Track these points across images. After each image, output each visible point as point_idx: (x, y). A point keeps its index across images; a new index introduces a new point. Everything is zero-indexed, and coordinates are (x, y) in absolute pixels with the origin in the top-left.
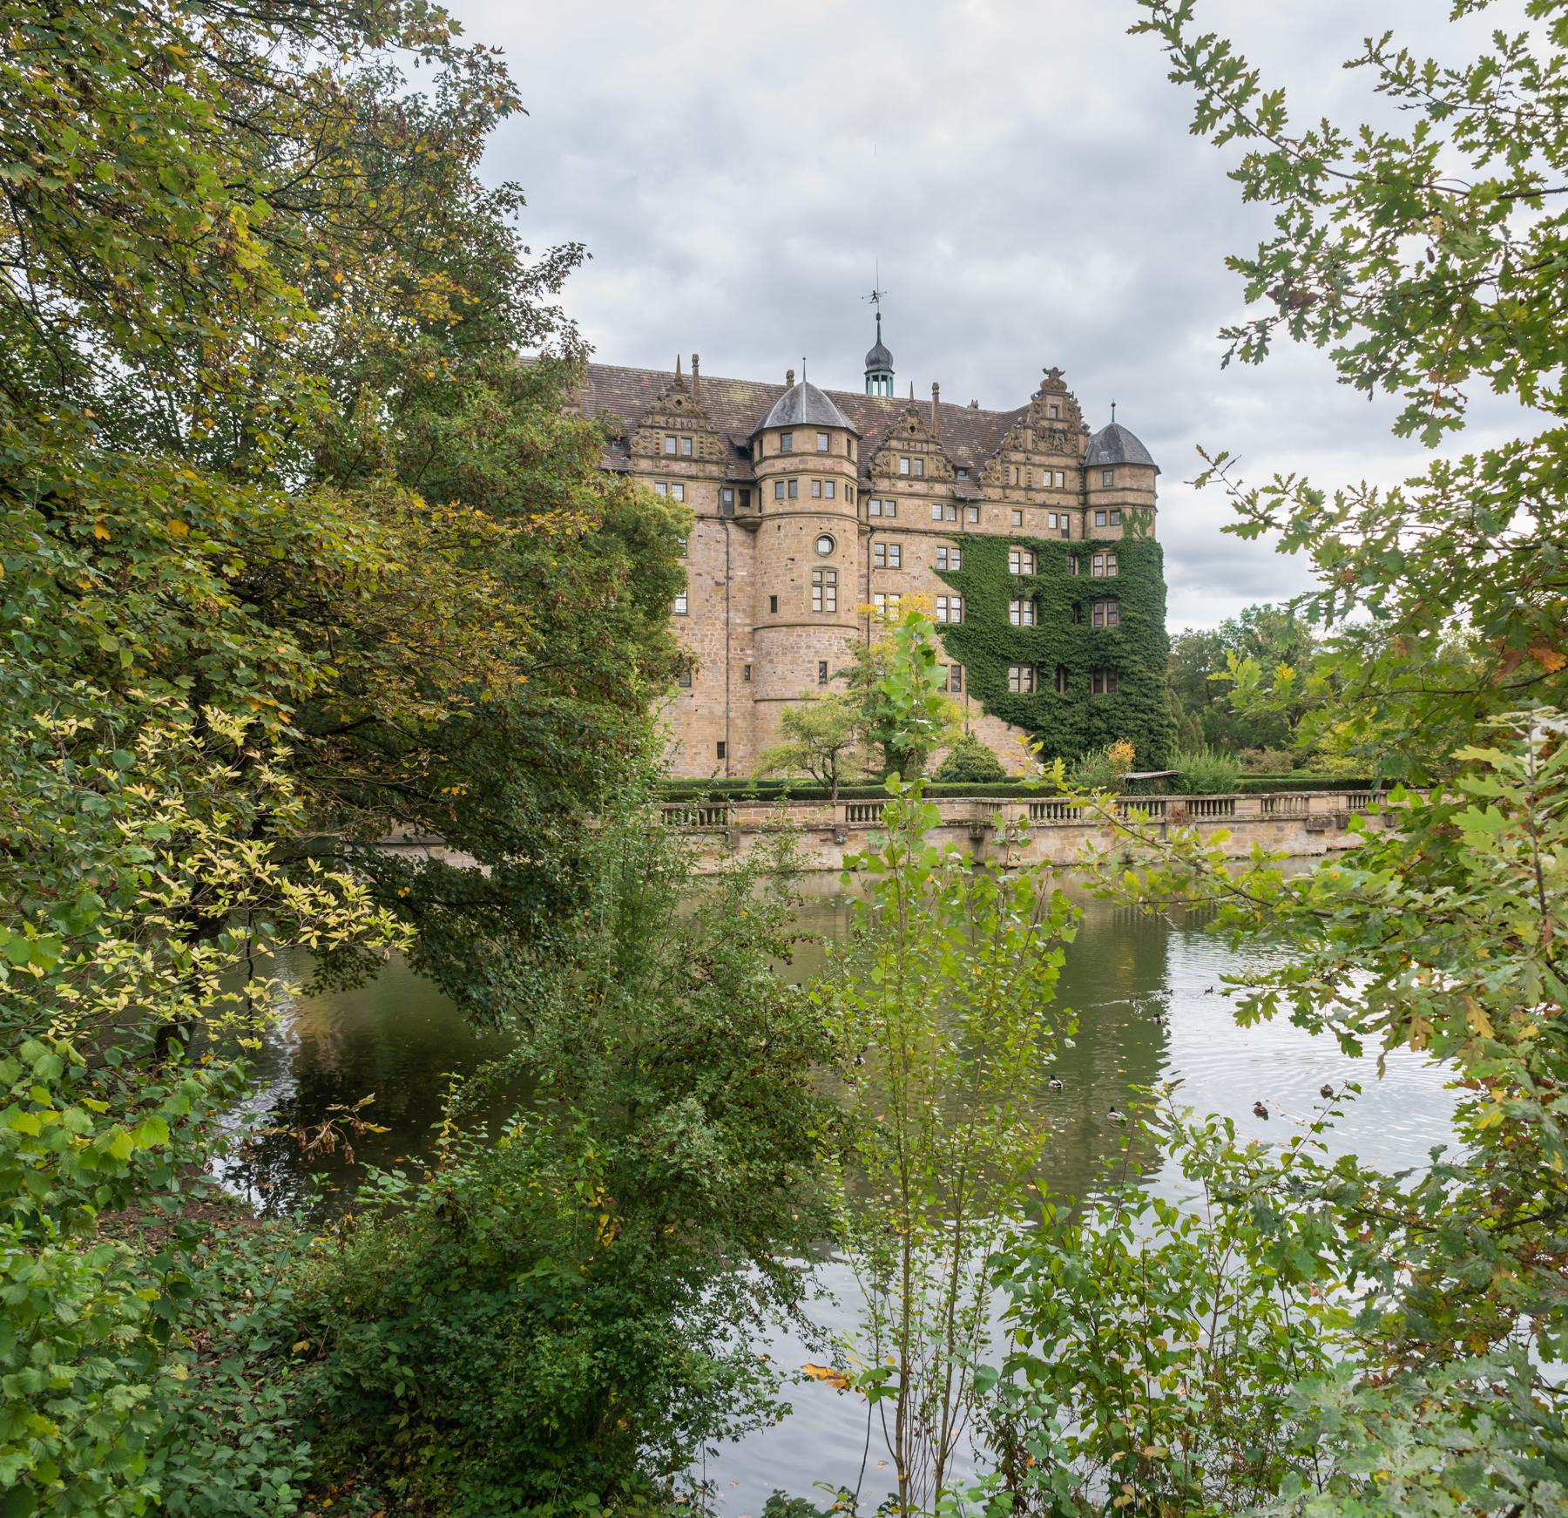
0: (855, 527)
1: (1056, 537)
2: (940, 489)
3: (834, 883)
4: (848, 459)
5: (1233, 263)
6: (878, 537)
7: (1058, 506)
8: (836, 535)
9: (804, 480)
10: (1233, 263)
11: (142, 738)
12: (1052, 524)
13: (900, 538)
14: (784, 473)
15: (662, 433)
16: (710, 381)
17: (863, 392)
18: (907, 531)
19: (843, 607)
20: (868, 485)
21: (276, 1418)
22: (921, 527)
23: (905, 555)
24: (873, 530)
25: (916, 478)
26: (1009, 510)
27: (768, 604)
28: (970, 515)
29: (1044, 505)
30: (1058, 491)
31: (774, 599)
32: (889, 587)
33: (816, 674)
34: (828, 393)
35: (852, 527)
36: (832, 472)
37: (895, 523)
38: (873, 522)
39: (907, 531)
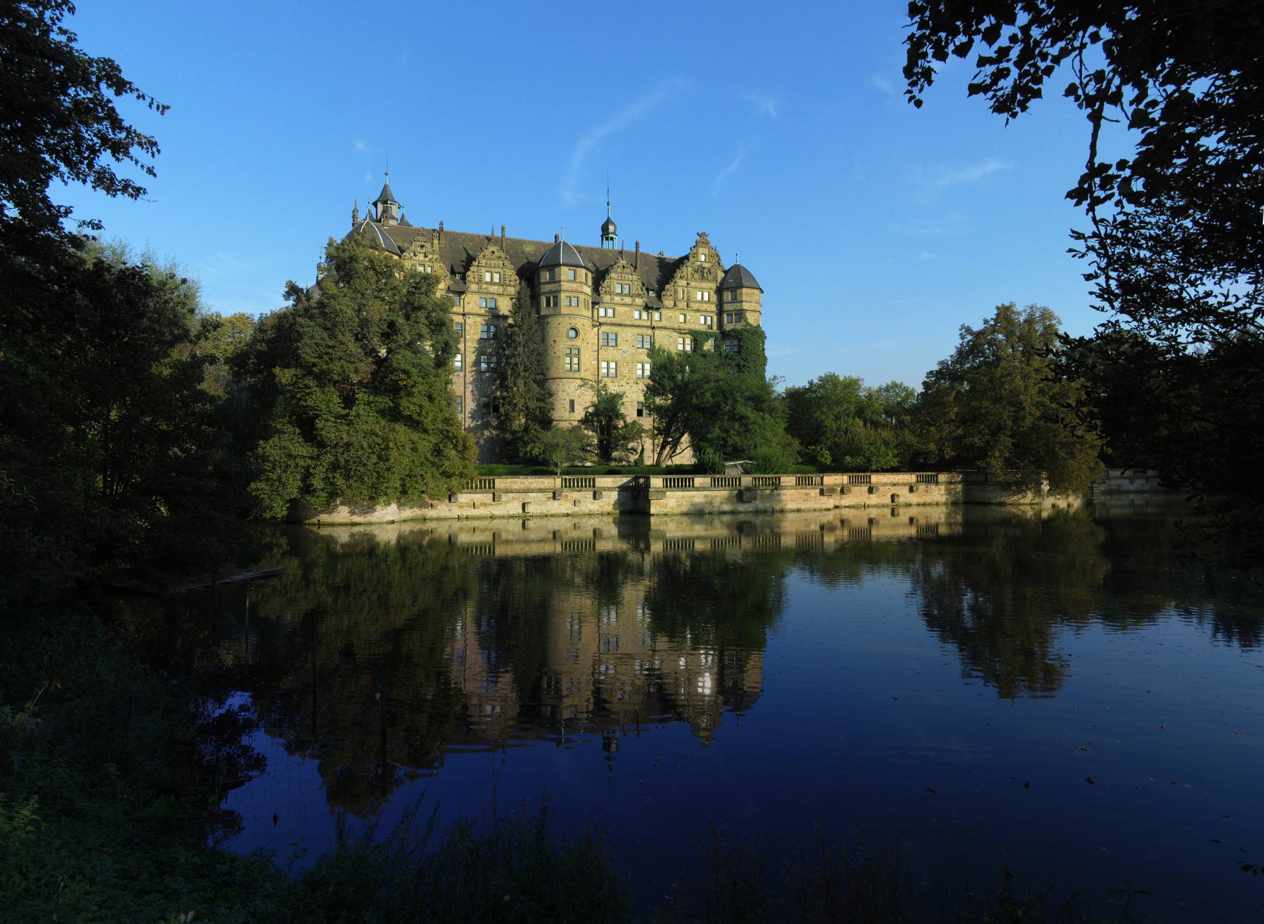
0: (590, 323)
1: (704, 329)
2: (639, 301)
4: (586, 283)
5: (441, 224)
6: (603, 328)
8: (579, 327)
9: (563, 295)
10: (441, 224)
11: (1045, 515)
13: (616, 329)
14: (551, 292)
19: (582, 368)
22: (628, 322)
26: (677, 313)
28: (656, 315)
29: (698, 311)
30: (495, 284)
32: (610, 357)
33: (568, 407)
34: (578, 248)
35: (588, 323)
36: (576, 291)
37: (613, 321)
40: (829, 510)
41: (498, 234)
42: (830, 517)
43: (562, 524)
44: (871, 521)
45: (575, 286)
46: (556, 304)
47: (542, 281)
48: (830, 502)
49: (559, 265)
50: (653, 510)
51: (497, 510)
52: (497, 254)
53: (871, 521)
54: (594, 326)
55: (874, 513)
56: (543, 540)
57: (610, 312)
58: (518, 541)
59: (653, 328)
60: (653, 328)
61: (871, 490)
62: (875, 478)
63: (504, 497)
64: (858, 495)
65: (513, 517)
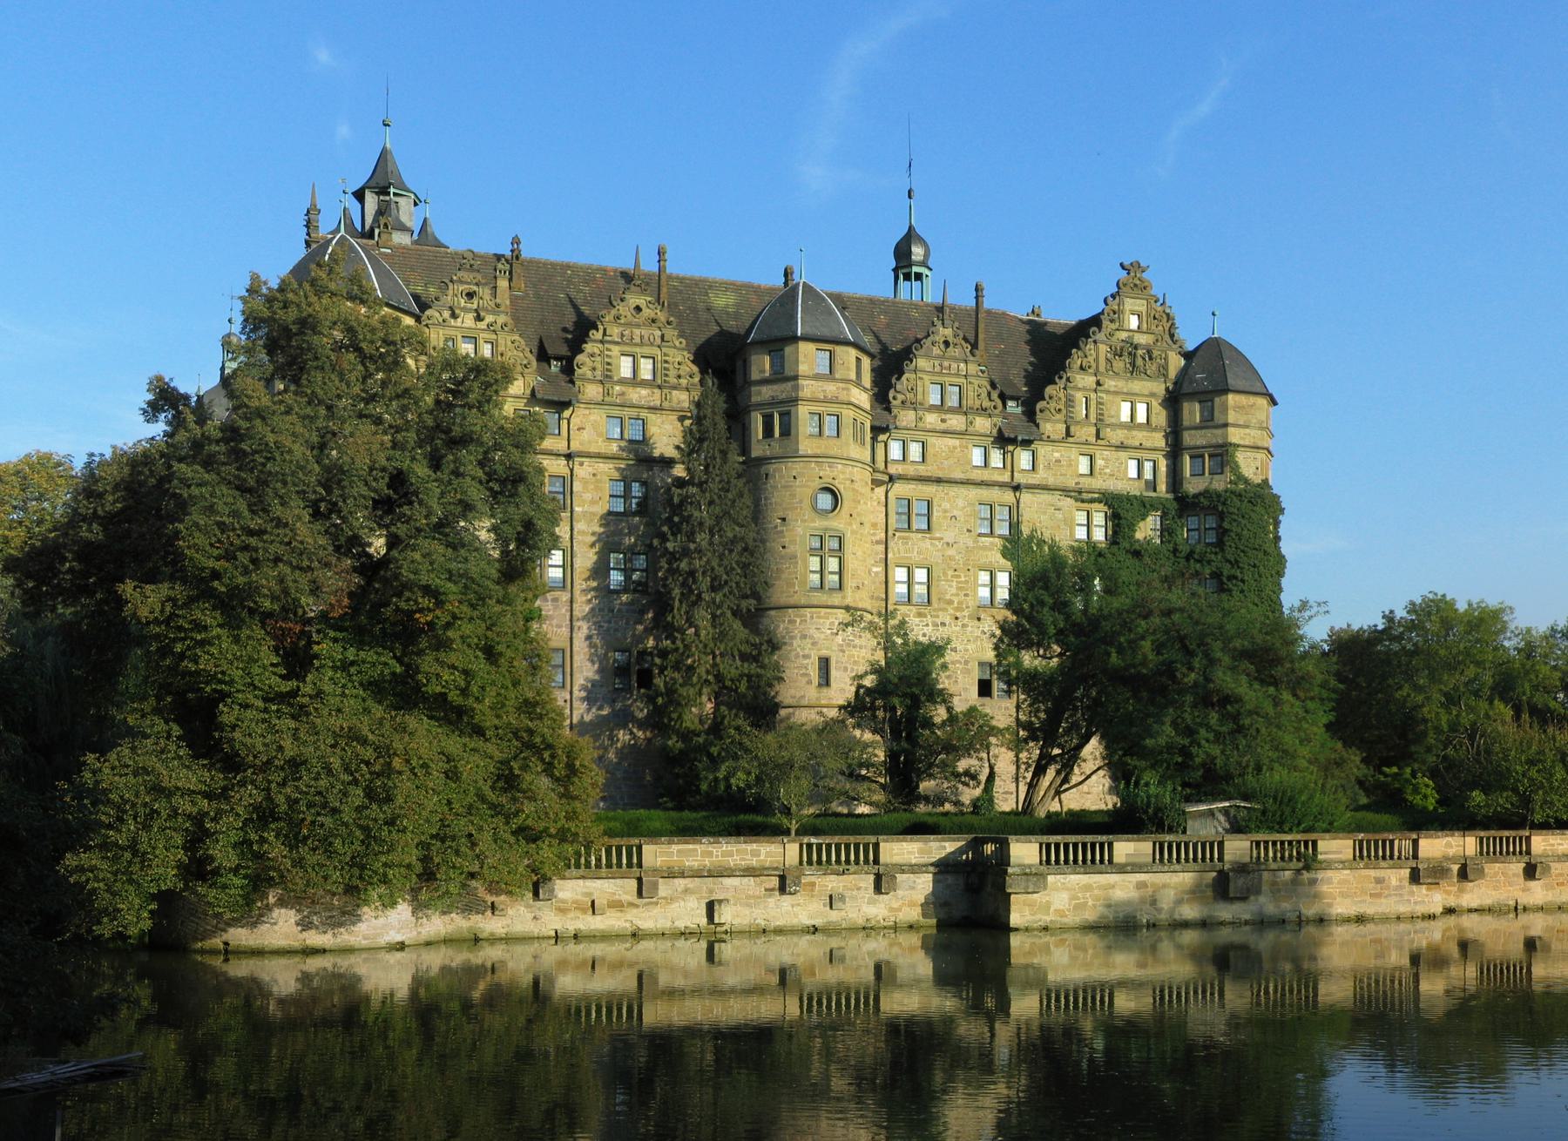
1: (1136, 489)
4: (858, 383)
6: (899, 489)
7: (1140, 447)
8: (840, 486)
9: (803, 411)
12: (1133, 473)
13: (929, 490)
14: (774, 403)
15: (616, 350)
16: (681, 280)
17: (889, 293)
18: (939, 481)
19: (850, 583)
21: (463, 406)
22: (958, 475)
24: (891, 479)
25: (952, 410)
26: (1073, 452)
27: (814, 673)
29: (1122, 447)
30: (644, 384)
31: (825, 664)
32: (915, 557)
34: (838, 298)
35: (863, 475)
37: (923, 470)
38: (892, 470)
39: (939, 481)
41: (649, 265)
42: (1435, 933)
44: (1531, 945)
45: (831, 388)
46: (786, 432)
49: (795, 339)
50: (1015, 919)
51: (649, 918)
52: (647, 312)
53: (1531, 945)
54: (876, 483)
55: (1537, 925)
56: (756, 990)
57: (915, 450)
58: (697, 992)
59: (1017, 488)
60: (1017, 488)
61: (1530, 872)
62: (1541, 843)
63: (665, 887)
64: (1501, 882)
65: (685, 934)
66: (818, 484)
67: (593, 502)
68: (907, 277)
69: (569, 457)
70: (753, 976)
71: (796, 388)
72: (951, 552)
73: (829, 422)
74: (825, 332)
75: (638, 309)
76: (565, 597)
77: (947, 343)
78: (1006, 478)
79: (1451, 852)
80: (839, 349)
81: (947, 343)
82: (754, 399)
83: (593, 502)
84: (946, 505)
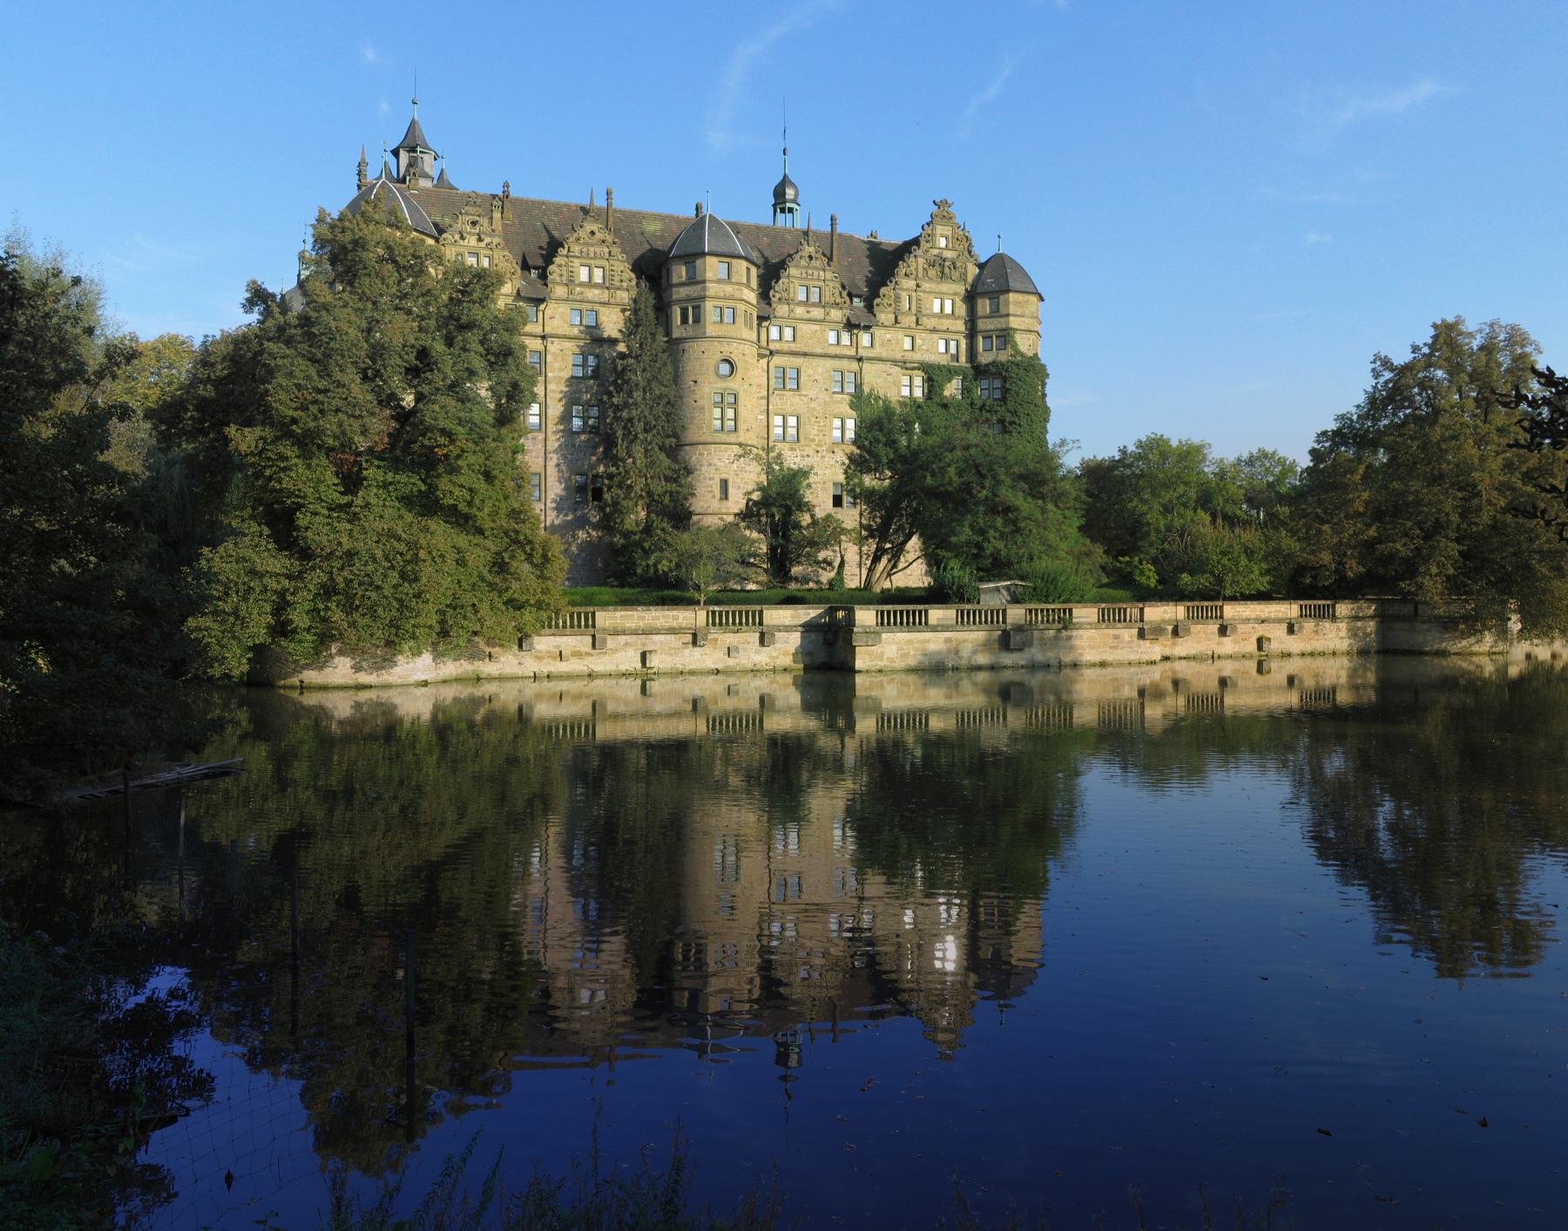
3: (695, 687)
4: (748, 285)
6: (777, 360)
8: (735, 358)
9: (709, 305)
14: (689, 299)
15: (577, 262)
19: (742, 427)
20: (766, 311)
23: (803, 378)
30: (597, 286)
32: (788, 408)
34: (734, 226)
38: (772, 346)
40: (1153, 663)
41: (600, 202)
42: (1155, 675)
43: (707, 688)
44: (1223, 682)
46: (697, 320)
47: (675, 280)
48: (1154, 650)
49: (703, 254)
51: (600, 664)
53: (1223, 682)
54: (761, 356)
55: (1228, 669)
56: (675, 714)
57: (788, 333)
58: (633, 716)
59: (860, 360)
60: (860, 360)
61: (1223, 631)
62: (1231, 610)
63: (611, 642)
64: (1202, 638)
65: (626, 675)
66: (720, 357)
67: (561, 370)
68: (783, 211)
69: (544, 337)
70: (674, 704)
71: (704, 289)
72: (813, 405)
73: (728, 313)
74: (725, 250)
75: (593, 233)
76: (541, 436)
77: (811, 257)
78: (852, 352)
79: (1167, 617)
80: (735, 262)
81: (811, 257)
82: (675, 297)
83: (561, 370)
84: (810, 372)
